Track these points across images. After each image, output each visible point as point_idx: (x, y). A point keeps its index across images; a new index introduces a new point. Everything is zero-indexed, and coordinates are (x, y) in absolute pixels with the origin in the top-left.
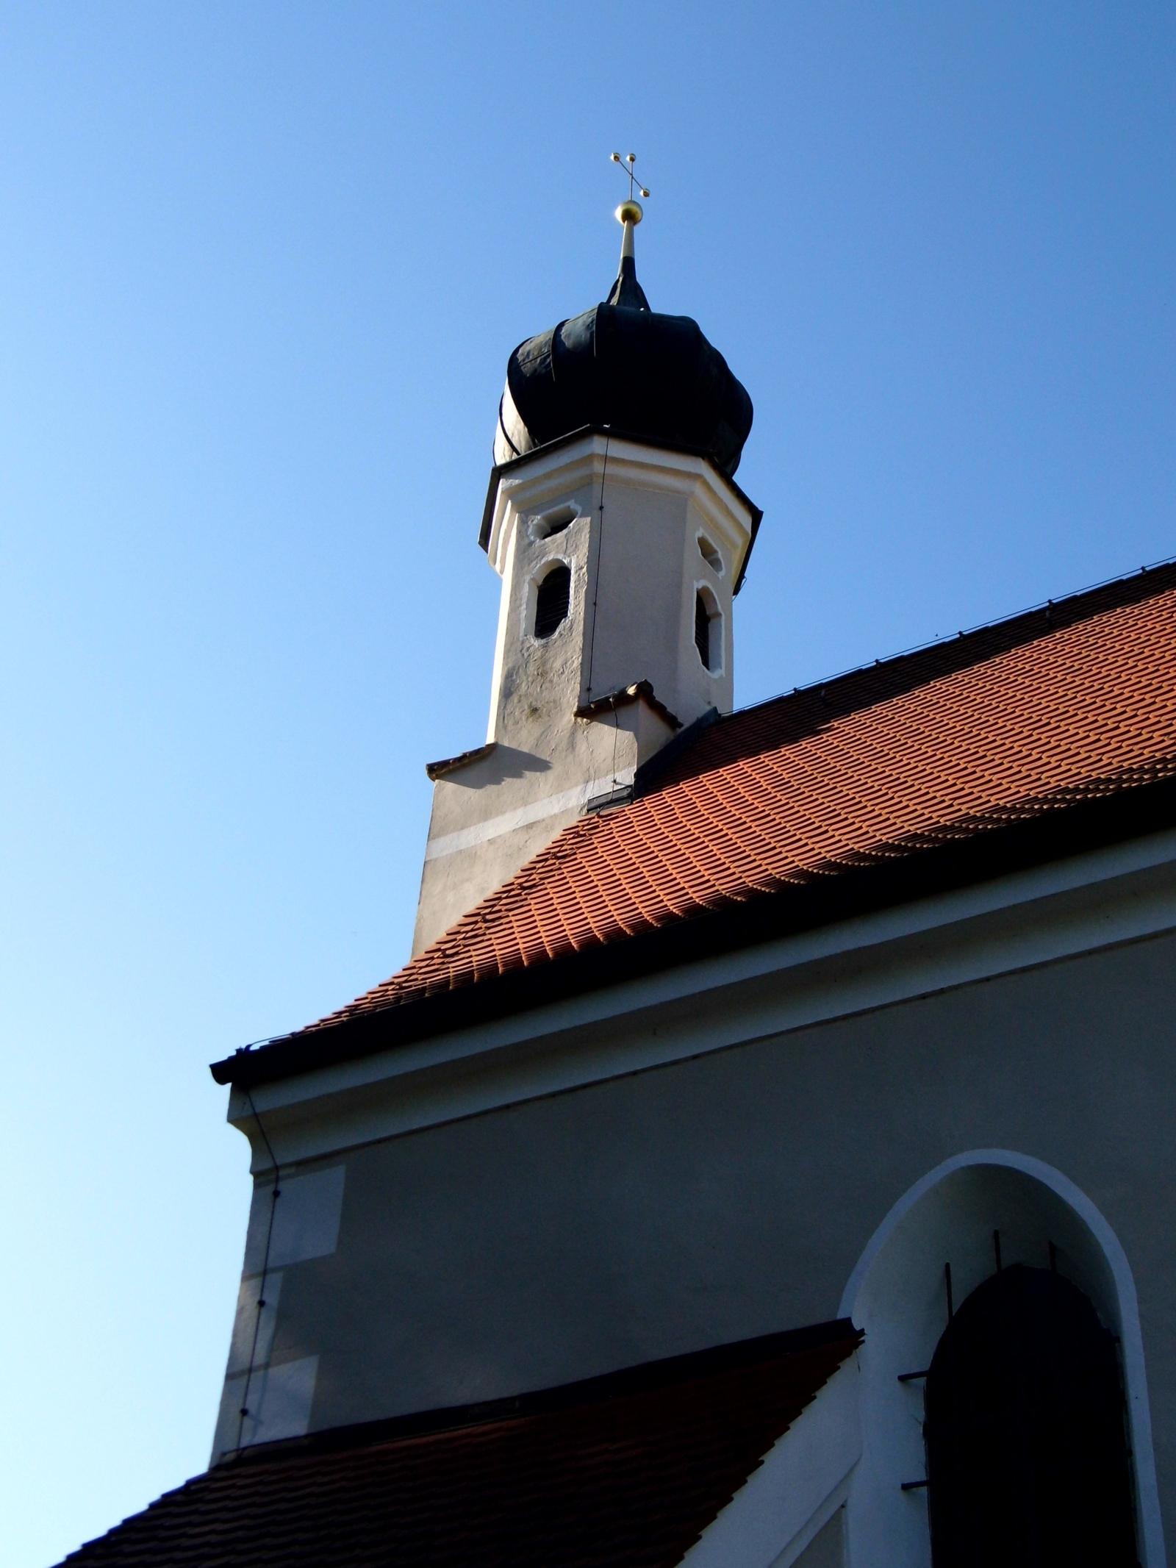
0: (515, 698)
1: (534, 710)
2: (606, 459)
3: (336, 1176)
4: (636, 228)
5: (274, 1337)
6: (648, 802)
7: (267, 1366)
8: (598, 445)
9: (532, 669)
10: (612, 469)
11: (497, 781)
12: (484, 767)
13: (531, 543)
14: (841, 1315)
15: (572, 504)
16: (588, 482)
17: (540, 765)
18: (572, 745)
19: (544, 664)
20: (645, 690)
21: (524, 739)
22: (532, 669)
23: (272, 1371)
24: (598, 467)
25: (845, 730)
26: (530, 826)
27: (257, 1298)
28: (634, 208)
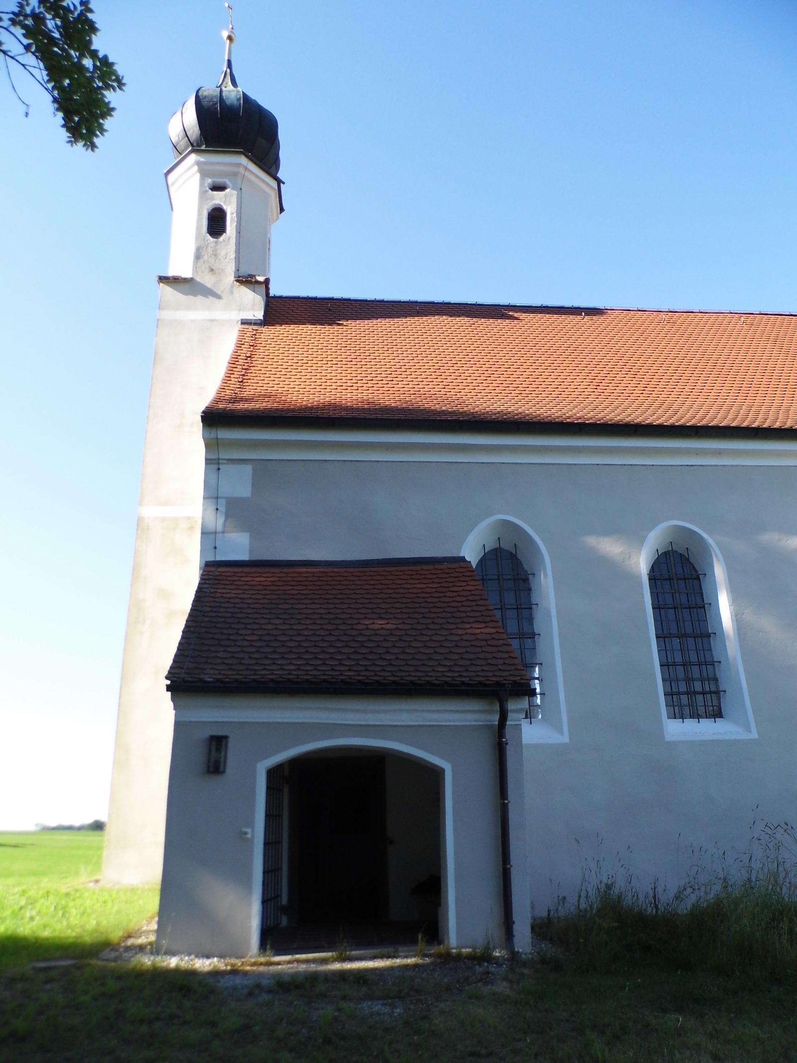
0: (201, 261)
1: (212, 270)
2: (246, 168)
3: (248, 469)
4: (233, 45)
5: (225, 521)
6: (264, 329)
7: (223, 532)
8: (243, 160)
9: (210, 250)
10: (247, 174)
11: (195, 295)
12: (186, 286)
13: (206, 191)
14: (461, 555)
15: (228, 182)
16: (235, 174)
17: (218, 297)
18: (231, 292)
19: (216, 250)
20: (267, 282)
21: (207, 280)
22: (210, 250)
23: (226, 535)
24: (242, 170)
25: (354, 327)
26: (212, 320)
27: (214, 507)
28: (233, 36)
